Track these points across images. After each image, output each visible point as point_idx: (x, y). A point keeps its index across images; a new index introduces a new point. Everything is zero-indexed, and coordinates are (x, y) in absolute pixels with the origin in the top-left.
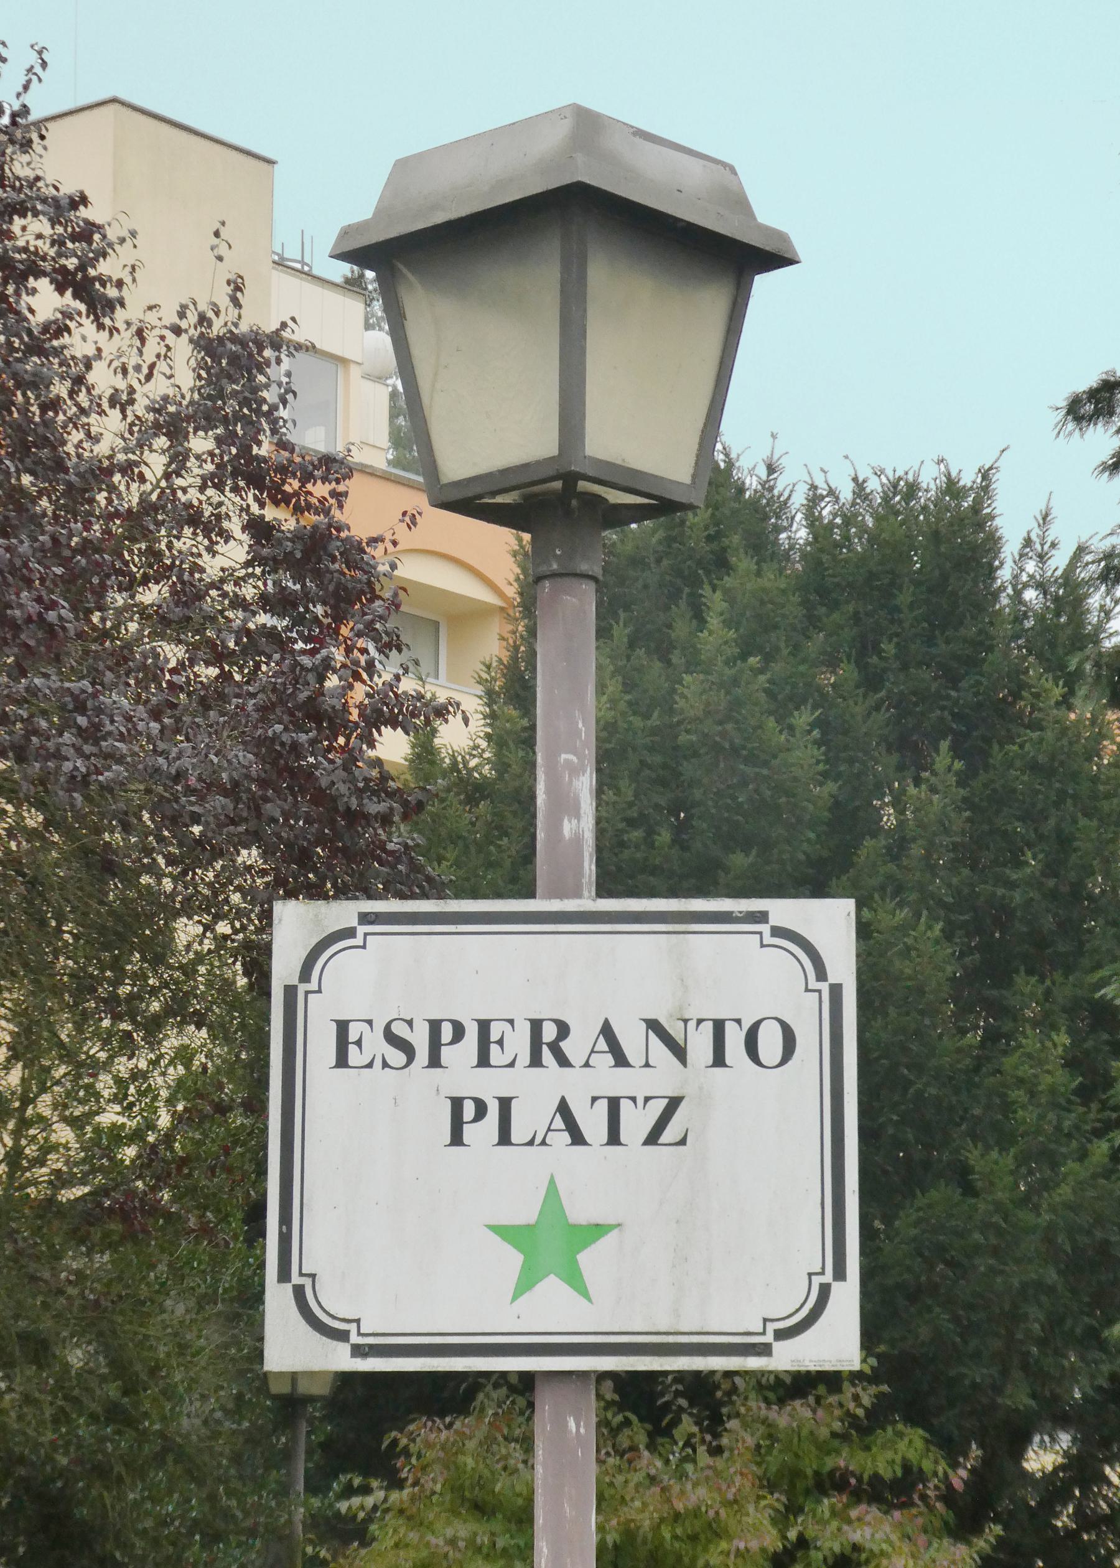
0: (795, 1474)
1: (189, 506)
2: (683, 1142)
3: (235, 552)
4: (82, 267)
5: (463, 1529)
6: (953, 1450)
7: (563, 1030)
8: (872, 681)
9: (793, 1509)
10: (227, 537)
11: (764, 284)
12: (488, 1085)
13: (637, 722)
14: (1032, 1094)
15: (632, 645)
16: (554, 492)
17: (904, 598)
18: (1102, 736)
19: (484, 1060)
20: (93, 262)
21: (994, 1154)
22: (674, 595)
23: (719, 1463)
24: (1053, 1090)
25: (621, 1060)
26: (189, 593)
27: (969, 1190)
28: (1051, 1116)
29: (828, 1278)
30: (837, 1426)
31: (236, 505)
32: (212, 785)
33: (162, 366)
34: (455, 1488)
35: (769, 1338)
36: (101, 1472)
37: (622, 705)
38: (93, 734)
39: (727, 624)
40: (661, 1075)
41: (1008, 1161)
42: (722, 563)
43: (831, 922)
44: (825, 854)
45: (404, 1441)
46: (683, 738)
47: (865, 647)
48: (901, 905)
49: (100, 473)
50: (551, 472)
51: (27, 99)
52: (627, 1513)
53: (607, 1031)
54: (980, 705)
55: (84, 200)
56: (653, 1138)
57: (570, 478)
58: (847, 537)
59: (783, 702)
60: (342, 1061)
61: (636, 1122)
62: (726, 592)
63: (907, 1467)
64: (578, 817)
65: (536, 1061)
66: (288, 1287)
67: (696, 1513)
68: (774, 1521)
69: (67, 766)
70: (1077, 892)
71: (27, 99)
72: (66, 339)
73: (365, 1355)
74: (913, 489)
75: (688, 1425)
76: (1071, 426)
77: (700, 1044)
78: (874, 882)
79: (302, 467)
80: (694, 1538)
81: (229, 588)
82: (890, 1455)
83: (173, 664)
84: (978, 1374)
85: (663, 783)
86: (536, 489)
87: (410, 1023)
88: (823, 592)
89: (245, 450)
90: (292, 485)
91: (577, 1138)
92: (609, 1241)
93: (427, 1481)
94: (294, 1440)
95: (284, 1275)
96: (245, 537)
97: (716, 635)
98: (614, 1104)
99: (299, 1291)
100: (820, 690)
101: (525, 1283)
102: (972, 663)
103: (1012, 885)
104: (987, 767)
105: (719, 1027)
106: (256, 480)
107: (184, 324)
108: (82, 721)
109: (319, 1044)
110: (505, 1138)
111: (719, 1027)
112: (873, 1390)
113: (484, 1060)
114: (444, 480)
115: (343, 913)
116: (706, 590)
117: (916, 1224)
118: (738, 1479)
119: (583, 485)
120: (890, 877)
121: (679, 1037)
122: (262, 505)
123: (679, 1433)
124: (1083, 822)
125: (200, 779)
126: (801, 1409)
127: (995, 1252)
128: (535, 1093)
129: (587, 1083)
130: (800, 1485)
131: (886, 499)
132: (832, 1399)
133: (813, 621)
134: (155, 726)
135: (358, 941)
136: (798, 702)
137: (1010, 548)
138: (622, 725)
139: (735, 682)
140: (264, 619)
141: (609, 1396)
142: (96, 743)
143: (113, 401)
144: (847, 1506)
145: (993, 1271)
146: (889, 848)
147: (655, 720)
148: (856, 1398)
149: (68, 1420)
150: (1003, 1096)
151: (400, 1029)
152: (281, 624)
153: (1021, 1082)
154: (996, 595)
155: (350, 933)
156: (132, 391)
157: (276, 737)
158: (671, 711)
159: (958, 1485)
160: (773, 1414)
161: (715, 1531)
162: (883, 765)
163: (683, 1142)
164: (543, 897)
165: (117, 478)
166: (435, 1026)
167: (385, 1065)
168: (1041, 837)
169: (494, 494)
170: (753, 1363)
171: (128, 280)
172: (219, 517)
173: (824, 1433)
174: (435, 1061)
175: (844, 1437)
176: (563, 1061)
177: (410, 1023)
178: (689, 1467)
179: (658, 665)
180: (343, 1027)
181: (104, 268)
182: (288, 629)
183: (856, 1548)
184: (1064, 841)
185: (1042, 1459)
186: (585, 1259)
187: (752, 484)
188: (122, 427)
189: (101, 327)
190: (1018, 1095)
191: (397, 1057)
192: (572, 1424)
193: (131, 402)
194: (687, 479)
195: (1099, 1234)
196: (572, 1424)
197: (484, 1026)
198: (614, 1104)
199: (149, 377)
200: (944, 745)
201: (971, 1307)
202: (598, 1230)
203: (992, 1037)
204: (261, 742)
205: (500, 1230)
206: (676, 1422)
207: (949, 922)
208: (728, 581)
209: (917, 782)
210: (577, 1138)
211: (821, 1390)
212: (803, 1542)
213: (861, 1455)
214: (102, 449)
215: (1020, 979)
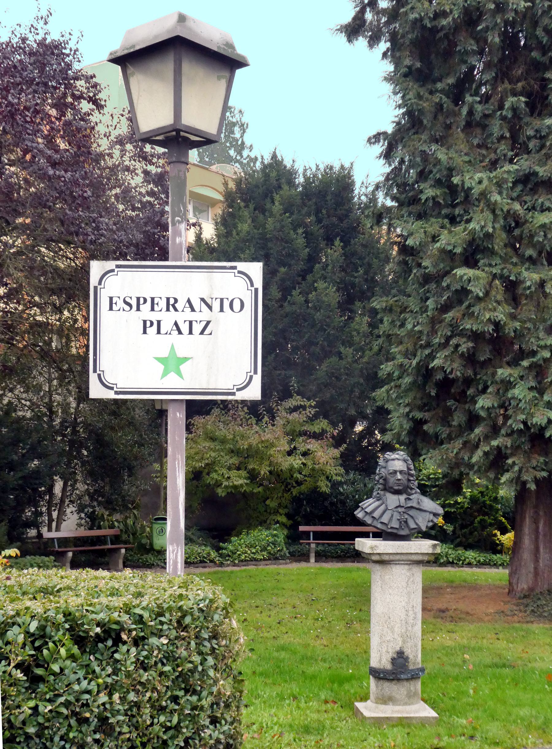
0: (294, 431)
1: (127, 166)
2: (211, 334)
3: (138, 179)
4: (94, 96)
5: (207, 444)
6: (334, 424)
7: (176, 301)
8: (319, 221)
9: (293, 440)
10: (137, 175)
11: (239, 73)
12: (154, 317)
13: (256, 231)
14: (359, 333)
15: (255, 210)
16: (173, 136)
17: (328, 198)
18: (381, 237)
19: (153, 309)
20: (97, 94)
21: (348, 349)
22: (266, 196)
23: (274, 428)
24: (364, 332)
25: (193, 310)
26: (127, 191)
27: (341, 358)
28: (363, 339)
29: (252, 373)
30: (305, 419)
31: (139, 166)
32: (131, 244)
33: (118, 125)
34: (206, 434)
35: (235, 391)
36: (112, 428)
37: (252, 226)
38: (97, 228)
39: (280, 204)
40: (204, 314)
41: (351, 350)
42: (280, 187)
43: (255, 270)
44: (306, 268)
45: (193, 422)
46: (268, 236)
47: (318, 211)
48: (325, 282)
49: (101, 155)
50: (171, 129)
51: (78, 46)
52: (250, 441)
53: (189, 301)
54: (348, 228)
55: (95, 76)
56: (202, 333)
57: (178, 131)
58: (314, 181)
59: (295, 227)
60: (111, 309)
61: (197, 328)
62: (280, 195)
63: (323, 430)
64: (181, 237)
65: (168, 310)
66: (96, 374)
67: (267, 441)
68: (288, 443)
69: (89, 238)
70: (373, 280)
71: (78, 46)
72: (91, 117)
73: (118, 394)
74: (331, 168)
75: (266, 418)
76: (368, 145)
77: (216, 306)
78: (319, 276)
79: (158, 155)
80: (267, 447)
81: (138, 189)
82: (318, 426)
83: (121, 210)
84: (342, 406)
85: (263, 249)
86: (168, 134)
87: (131, 298)
88: (307, 196)
89: (141, 150)
90: (155, 160)
91: (180, 332)
92: (189, 363)
93: (198, 432)
94: (162, 421)
95: (95, 371)
96: (142, 175)
97: (277, 208)
98: (191, 323)
99: (99, 375)
100: (305, 223)
101: (165, 374)
102: (347, 216)
103: (356, 277)
104: (350, 245)
105: (222, 300)
106: (145, 158)
107: (124, 113)
108: (94, 225)
109: (104, 304)
110: (159, 332)
111: (222, 300)
112: (314, 410)
113: (153, 309)
114: (141, 132)
115: (111, 264)
116: (275, 195)
117: (327, 367)
118: (278, 433)
119: (182, 134)
120: (322, 274)
121: (210, 303)
122: (146, 166)
123: (264, 420)
124: (374, 260)
125: (127, 242)
126: (295, 415)
127: (347, 374)
128: (168, 319)
129: (183, 316)
130: (295, 434)
131: (325, 170)
132: (304, 412)
133: (304, 204)
134: (114, 227)
135: (115, 273)
136: (299, 226)
137: (357, 185)
138: (252, 232)
139: (282, 220)
140: (148, 198)
141: (246, 411)
142: (98, 231)
143: (105, 136)
144: (307, 439)
145: (346, 379)
146: (323, 267)
147: (260, 231)
148: (310, 412)
149: (102, 415)
150: (350, 333)
151: (128, 300)
152: (152, 200)
153: (356, 330)
154: (354, 198)
155: (113, 271)
156: (110, 132)
157: (148, 231)
158: (265, 228)
159: (335, 434)
160: (288, 416)
161: (272, 445)
162: (323, 244)
163: (211, 334)
164: (173, 261)
165: (106, 157)
166: (138, 299)
167: (124, 310)
168: (364, 264)
169: (156, 136)
170: (230, 398)
171: (107, 100)
172: (135, 169)
173: (301, 421)
174: (138, 309)
175: (307, 422)
176: (176, 310)
177: (131, 298)
178: (266, 429)
179: (262, 216)
180: (111, 299)
181: (100, 96)
182: (154, 201)
183: (309, 450)
184: (370, 265)
185: (359, 428)
186: (183, 367)
187: (289, 166)
188: (108, 143)
189: (100, 113)
190: (355, 333)
191: (127, 308)
192: (178, 414)
193: (110, 135)
194: (215, 133)
195: (374, 370)
196: (178, 414)
197: (153, 299)
198: (191, 323)
199: (115, 129)
200: (338, 239)
201: (341, 389)
202: (186, 359)
203: (350, 318)
204: (145, 232)
205: (158, 359)
206: (263, 418)
207: (338, 286)
208: (281, 192)
209: (331, 249)
210: (180, 332)
211: (301, 410)
212: (295, 448)
213: (311, 427)
214: (102, 149)
215: (356, 303)
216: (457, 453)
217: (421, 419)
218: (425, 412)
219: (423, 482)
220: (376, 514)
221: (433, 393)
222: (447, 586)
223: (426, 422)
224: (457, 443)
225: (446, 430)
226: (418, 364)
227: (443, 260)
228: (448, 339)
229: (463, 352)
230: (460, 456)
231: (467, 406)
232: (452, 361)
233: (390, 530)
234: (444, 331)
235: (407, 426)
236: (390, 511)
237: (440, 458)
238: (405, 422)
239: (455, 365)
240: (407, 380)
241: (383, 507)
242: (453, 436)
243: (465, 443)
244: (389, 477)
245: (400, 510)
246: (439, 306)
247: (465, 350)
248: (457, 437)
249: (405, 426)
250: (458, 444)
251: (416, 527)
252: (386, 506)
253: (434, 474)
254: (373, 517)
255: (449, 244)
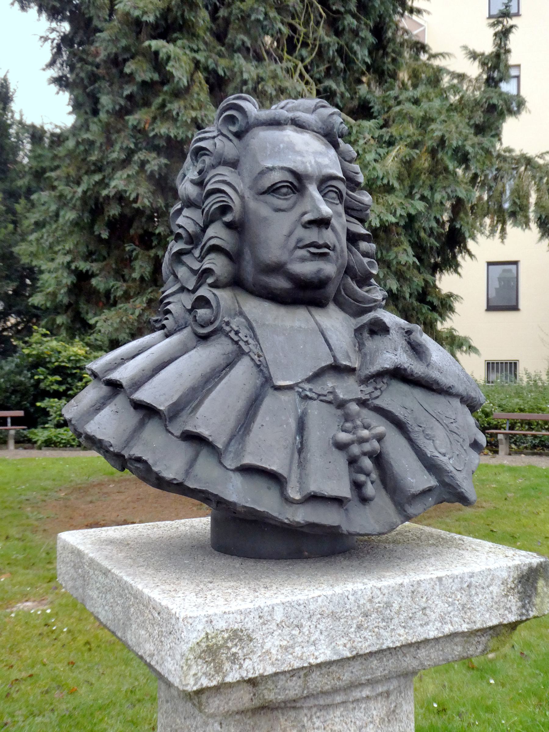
216: (140, 315)
217: (87, 271)
218: (92, 262)
219: (63, 364)
220: (212, 419)
221: (105, 235)
222: (109, 481)
223: (93, 275)
224: (138, 302)
225: (122, 286)
226: (85, 192)
227: (125, 35)
228: (131, 153)
229: (152, 172)
230: (145, 318)
231: (152, 253)
232: (138, 184)
233: (301, 516)
234: (124, 141)
235: (68, 280)
236: (285, 397)
237: (118, 320)
238: (65, 274)
239: (142, 190)
240: (70, 215)
241: (242, 375)
242: (132, 294)
243: (150, 302)
244: (260, 208)
245: (347, 389)
246: (117, 107)
247: (156, 168)
248: (138, 294)
249: (64, 281)
250: (140, 303)
251: (432, 482)
252: (261, 367)
253: (75, 356)
254: (192, 438)
255: (136, 8)
